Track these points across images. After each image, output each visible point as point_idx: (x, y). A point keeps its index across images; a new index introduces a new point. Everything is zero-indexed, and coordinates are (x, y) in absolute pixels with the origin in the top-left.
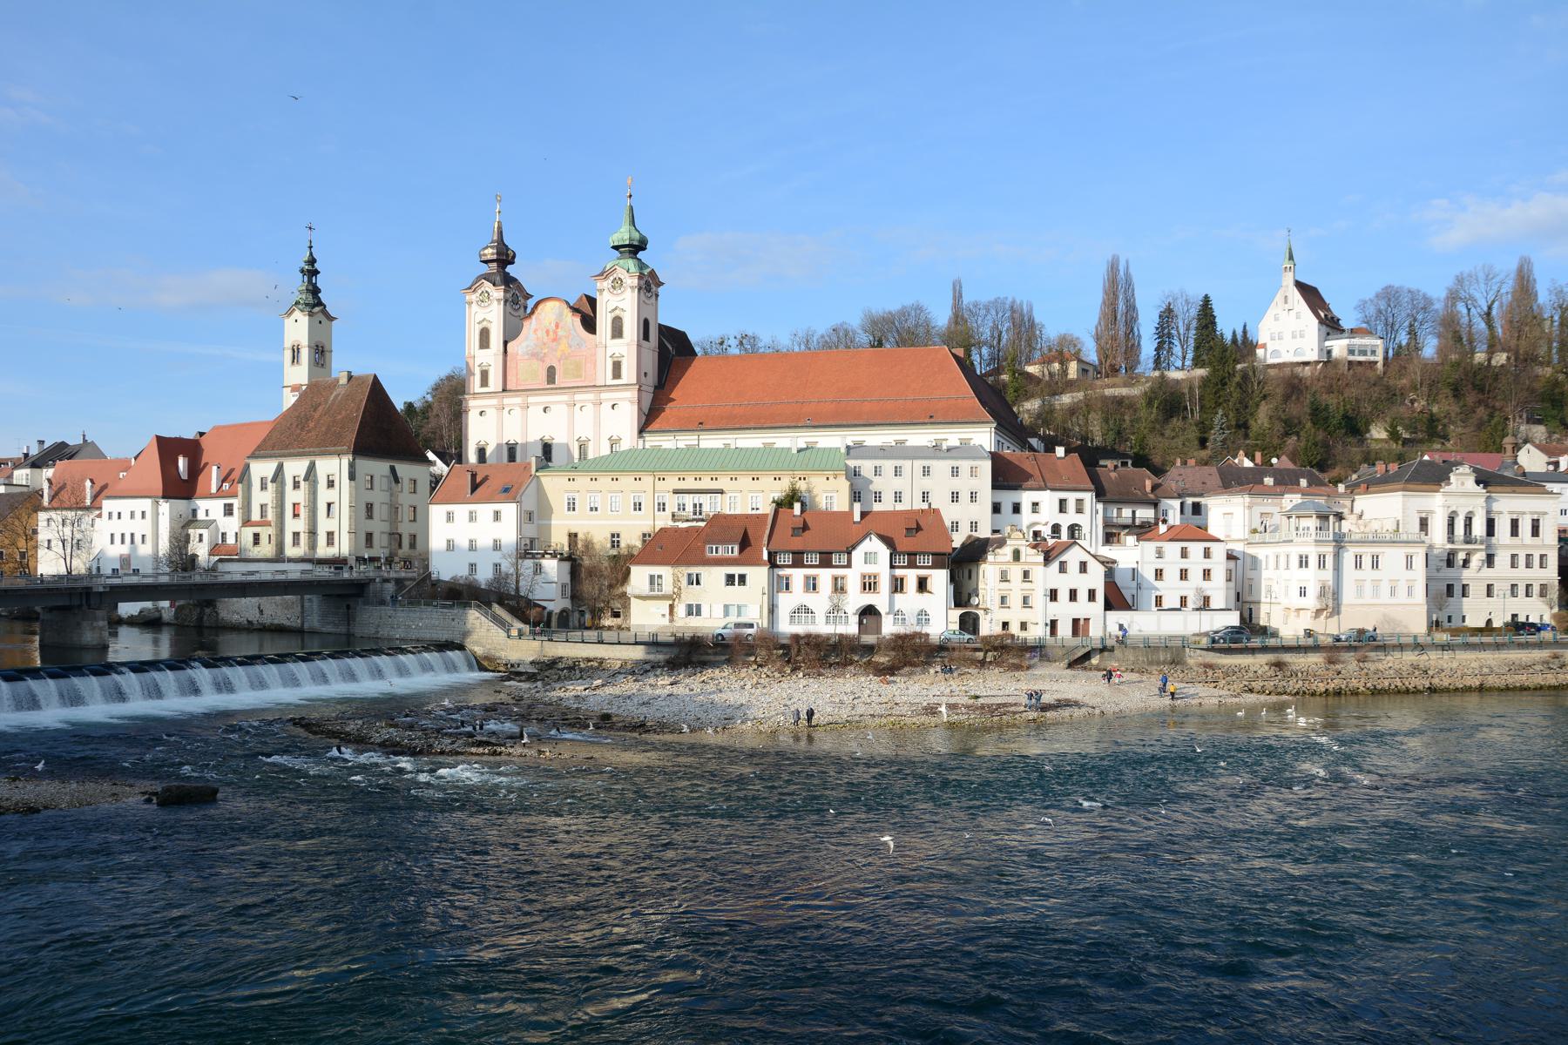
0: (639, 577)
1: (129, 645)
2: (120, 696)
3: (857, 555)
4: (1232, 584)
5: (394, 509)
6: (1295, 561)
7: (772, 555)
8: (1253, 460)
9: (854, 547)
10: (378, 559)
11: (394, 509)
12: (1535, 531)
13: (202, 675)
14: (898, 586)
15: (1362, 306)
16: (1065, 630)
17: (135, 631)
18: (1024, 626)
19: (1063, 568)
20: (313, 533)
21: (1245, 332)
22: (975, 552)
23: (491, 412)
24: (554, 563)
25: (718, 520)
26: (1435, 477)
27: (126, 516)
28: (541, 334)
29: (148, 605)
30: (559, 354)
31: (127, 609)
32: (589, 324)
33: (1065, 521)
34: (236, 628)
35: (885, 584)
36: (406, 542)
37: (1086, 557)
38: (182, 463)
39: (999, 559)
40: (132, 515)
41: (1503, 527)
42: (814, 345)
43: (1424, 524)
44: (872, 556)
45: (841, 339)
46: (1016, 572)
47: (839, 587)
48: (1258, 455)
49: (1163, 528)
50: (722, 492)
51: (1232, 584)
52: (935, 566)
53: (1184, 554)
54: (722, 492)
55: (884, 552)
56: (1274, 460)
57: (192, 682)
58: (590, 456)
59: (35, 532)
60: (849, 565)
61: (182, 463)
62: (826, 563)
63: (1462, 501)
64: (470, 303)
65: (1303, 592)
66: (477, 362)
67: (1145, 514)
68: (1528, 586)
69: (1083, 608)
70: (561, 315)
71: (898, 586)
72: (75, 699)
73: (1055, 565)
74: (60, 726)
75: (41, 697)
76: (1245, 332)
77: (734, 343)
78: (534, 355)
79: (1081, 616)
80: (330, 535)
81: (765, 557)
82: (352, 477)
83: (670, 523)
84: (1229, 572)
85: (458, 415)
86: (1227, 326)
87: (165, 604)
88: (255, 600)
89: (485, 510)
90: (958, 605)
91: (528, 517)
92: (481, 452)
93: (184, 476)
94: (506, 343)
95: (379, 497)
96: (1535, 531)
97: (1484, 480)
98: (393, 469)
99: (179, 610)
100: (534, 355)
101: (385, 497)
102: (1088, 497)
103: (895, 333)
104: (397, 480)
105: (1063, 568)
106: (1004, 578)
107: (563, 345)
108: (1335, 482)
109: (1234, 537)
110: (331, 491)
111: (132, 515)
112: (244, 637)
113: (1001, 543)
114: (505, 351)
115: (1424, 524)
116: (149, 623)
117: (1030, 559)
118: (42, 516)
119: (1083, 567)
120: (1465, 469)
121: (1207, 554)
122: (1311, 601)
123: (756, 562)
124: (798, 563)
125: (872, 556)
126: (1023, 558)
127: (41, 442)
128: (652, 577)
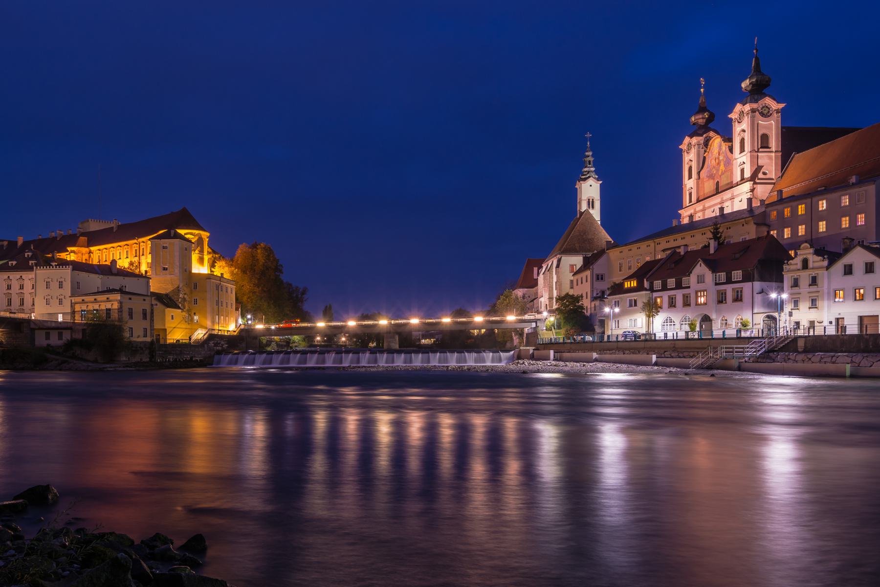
14: (721, 299)
28: (713, 162)
39: (792, 267)
46: (805, 277)
62: (679, 286)
73: (839, 266)
114: (699, 178)
117: (817, 264)
124: (664, 288)
126: (811, 265)
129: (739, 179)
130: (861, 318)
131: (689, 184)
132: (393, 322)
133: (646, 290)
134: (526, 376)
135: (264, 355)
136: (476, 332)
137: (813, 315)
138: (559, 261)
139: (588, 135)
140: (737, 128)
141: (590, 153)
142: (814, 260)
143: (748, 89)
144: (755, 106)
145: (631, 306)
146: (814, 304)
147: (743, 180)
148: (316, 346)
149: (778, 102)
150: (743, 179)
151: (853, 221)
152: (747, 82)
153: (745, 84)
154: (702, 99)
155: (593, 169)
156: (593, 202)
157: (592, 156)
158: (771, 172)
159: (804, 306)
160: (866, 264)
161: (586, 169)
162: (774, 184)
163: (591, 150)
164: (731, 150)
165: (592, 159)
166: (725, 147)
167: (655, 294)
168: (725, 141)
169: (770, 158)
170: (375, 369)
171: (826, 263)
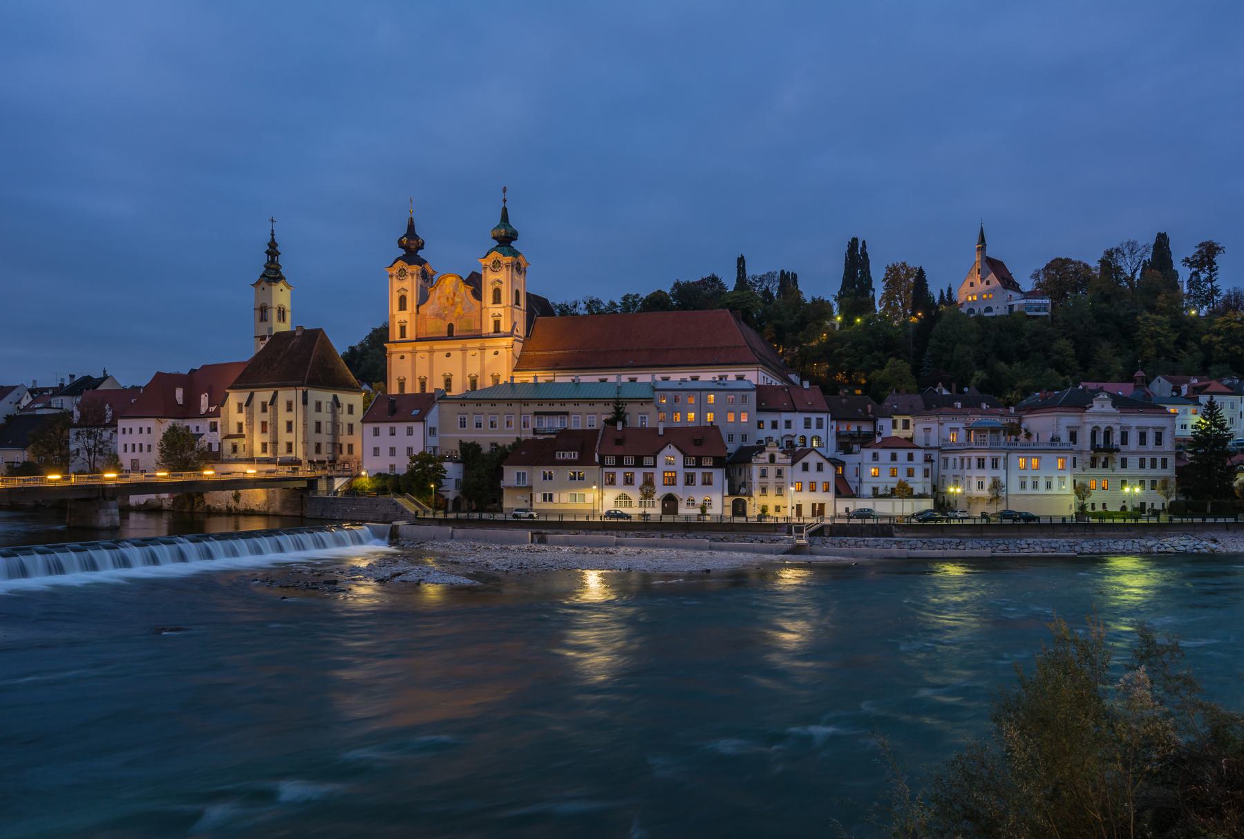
0: (510, 475)
1: (137, 525)
2: (125, 563)
3: (661, 459)
4: (929, 479)
5: (335, 425)
6: (974, 462)
7: (602, 458)
8: (950, 390)
9: (658, 453)
10: (324, 462)
11: (335, 425)
12: (1159, 441)
13: (188, 546)
14: (690, 480)
15: (1036, 276)
16: (807, 511)
17: (142, 517)
18: (777, 509)
19: (806, 467)
20: (275, 443)
21: (950, 290)
22: (744, 456)
23: (408, 356)
25: (564, 433)
26: (1081, 403)
27: (136, 431)
28: (443, 300)
29: (153, 496)
31: (134, 500)
32: (478, 294)
33: (813, 431)
34: (219, 513)
35: (681, 479)
36: (345, 449)
37: (821, 460)
39: (761, 461)
40: (141, 430)
41: (1133, 437)
43: (1073, 437)
44: (671, 458)
45: (656, 302)
46: (772, 471)
47: (648, 482)
48: (954, 386)
49: (878, 439)
51: (929, 479)
52: (715, 466)
53: (894, 457)
54: (567, 414)
55: (678, 459)
56: (966, 389)
58: (478, 388)
59: (67, 443)
60: (655, 466)
61: (179, 393)
62: (639, 463)
63: (1104, 419)
64: (391, 276)
65: (981, 486)
66: (397, 320)
67: (866, 428)
68: (134, 450)
69: (819, 497)
70: (456, 286)
71: (690, 480)
72: (59, 569)
73: (799, 465)
74: (114, 581)
75: (64, 564)
76: (950, 290)
77: (583, 306)
78: (438, 316)
81: (597, 460)
82: (305, 402)
83: (531, 436)
84: (926, 471)
85: (383, 357)
86: (935, 291)
87: (166, 496)
89: (401, 428)
90: (731, 493)
92: (1166, 581)
93: (180, 402)
94: (418, 307)
95: (325, 417)
96: (1159, 441)
97: (1118, 402)
98: (335, 397)
99: (176, 500)
100: (438, 316)
102: (825, 417)
103: (694, 297)
104: (338, 405)
105: (806, 467)
106: (764, 474)
107: (458, 310)
108: (1007, 406)
109: (932, 445)
111: (141, 430)
112: (224, 519)
113: (762, 450)
115: (1073, 437)
116: (151, 510)
117: (782, 461)
118: (73, 432)
119: (820, 467)
120: (1103, 396)
121: (910, 457)
122: (985, 493)
123: (592, 463)
124: (619, 463)
125: (671, 458)
126: (777, 460)
127: (72, 376)
129: (491, 329)
130: (814, 505)
133: (596, 464)
137: (779, 501)
139: (844, 401)
142: (779, 456)
146: (780, 491)
150: (497, 330)
151: (738, 418)
159: (771, 493)
170: (714, 536)
171: (789, 461)
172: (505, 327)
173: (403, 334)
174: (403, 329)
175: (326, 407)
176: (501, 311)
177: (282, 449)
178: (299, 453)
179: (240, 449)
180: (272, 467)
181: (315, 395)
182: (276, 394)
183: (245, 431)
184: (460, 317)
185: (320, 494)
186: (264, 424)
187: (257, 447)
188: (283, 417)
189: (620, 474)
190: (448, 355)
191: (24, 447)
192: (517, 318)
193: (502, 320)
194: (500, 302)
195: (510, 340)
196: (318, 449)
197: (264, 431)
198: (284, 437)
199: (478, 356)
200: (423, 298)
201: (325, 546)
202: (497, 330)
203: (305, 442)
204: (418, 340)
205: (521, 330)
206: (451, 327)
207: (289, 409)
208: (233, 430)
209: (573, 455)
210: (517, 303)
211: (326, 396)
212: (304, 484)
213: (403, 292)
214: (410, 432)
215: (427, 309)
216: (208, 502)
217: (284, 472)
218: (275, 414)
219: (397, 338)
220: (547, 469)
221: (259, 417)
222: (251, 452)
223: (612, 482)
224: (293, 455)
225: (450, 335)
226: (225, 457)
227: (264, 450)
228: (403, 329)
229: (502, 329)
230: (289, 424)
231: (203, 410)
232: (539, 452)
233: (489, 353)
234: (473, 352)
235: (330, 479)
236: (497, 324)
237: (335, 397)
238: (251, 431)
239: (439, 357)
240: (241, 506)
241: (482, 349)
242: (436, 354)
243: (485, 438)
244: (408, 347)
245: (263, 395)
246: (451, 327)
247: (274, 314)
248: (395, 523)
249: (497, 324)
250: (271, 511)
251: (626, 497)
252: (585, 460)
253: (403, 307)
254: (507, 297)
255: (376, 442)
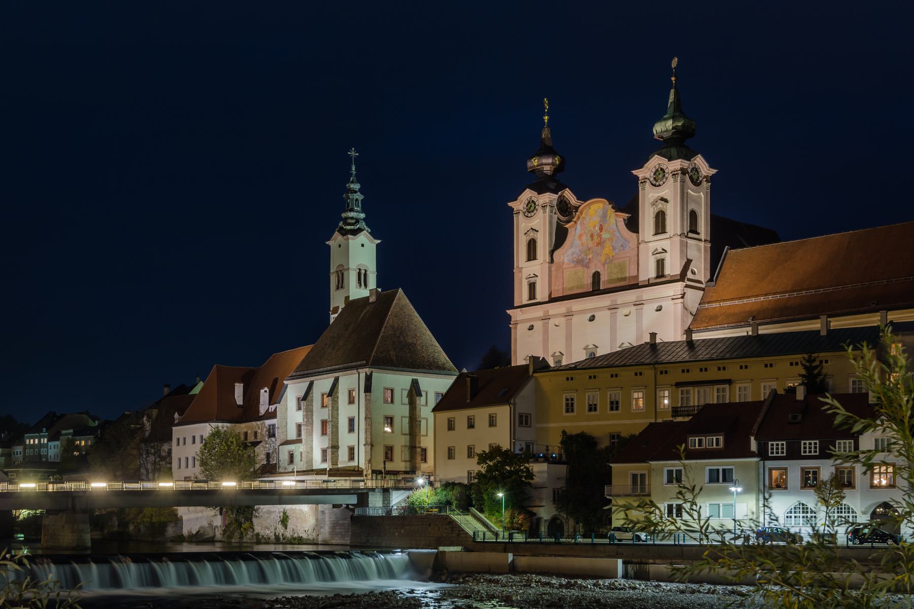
20: (335, 447)
23: (538, 325)
24: (544, 466)
30: (603, 258)
38: (239, 389)
42: (658, 341)
50: (729, 382)
54: (729, 382)
57: (154, 574)
61: (239, 389)
70: (604, 216)
78: (580, 262)
79: (639, 472)
80: (351, 449)
81: (754, 446)
82: (368, 389)
88: (686, 543)
89: (481, 414)
91: (521, 421)
94: (552, 253)
98: (415, 383)
100: (580, 262)
101: (405, 410)
107: (607, 250)
110: (352, 406)
114: (552, 261)
124: (794, 454)
128: (634, 476)
129: (652, 274)
131: (526, 270)
132: (51, 488)
133: (752, 455)
134: (238, 606)
135: (862, 577)
136: (24, 513)
138: (369, 378)
139: (353, 153)
140: (648, 196)
141: (356, 187)
143: (665, 135)
144: (686, 164)
145: (711, 481)
147: (661, 278)
148: (300, 541)
149: (711, 167)
150: (660, 274)
152: (669, 124)
153: (663, 127)
154: (546, 133)
155: (363, 216)
156: (365, 275)
157: (361, 191)
158: (699, 271)
160: (495, 426)
161: (351, 214)
162: (703, 289)
163: (358, 181)
164: (633, 225)
165: (359, 196)
166: (617, 220)
167: (769, 464)
168: (618, 208)
169: (699, 250)
172: (673, 268)
173: (532, 295)
174: (532, 287)
175: (401, 397)
176: (666, 244)
177: (343, 454)
178: (361, 461)
179: (297, 458)
180: (326, 477)
181: (385, 379)
182: (336, 380)
183: (303, 437)
184: (609, 261)
185: (371, 512)
186: (324, 423)
187: (317, 456)
188: (345, 411)
189: (794, 469)
190: (592, 319)
191: (457, 545)
192: (691, 254)
193: (667, 257)
194: (664, 232)
195: (678, 287)
196: (389, 453)
197: (324, 433)
198: (346, 439)
199: (633, 317)
200: (560, 237)
201: (333, 578)
202: (660, 274)
203: (371, 445)
204: (552, 300)
205: (700, 269)
206: (596, 276)
207: (351, 401)
208: (292, 435)
209: (715, 441)
210: (694, 230)
211: (401, 381)
212: (353, 500)
213: (532, 235)
214: (492, 422)
215: (565, 254)
216: (257, 529)
217: (343, 483)
218: (335, 408)
219: (525, 299)
220: (674, 465)
221: (320, 414)
222: (310, 461)
223: (781, 486)
224: (354, 464)
225: (596, 290)
226: (281, 470)
227: (324, 460)
228: (532, 287)
229: (668, 271)
230: (351, 421)
231: (262, 411)
232: (659, 442)
233: (649, 310)
234: (626, 311)
235: (386, 491)
236: (660, 264)
237: (415, 383)
238: (310, 433)
239: (580, 321)
240: (288, 534)
241: (639, 304)
242: (575, 319)
243: (601, 425)
244: (538, 312)
245: (323, 384)
246: (596, 276)
247: (353, 278)
248: (441, 549)
249: (660, 264)
250: (320, 539)
251: (805, 510)
252: (735, 448)
253: (532, 255)
254: (674, 222)
255: (450, 439)
